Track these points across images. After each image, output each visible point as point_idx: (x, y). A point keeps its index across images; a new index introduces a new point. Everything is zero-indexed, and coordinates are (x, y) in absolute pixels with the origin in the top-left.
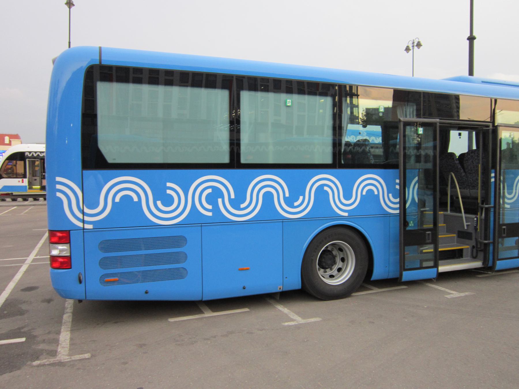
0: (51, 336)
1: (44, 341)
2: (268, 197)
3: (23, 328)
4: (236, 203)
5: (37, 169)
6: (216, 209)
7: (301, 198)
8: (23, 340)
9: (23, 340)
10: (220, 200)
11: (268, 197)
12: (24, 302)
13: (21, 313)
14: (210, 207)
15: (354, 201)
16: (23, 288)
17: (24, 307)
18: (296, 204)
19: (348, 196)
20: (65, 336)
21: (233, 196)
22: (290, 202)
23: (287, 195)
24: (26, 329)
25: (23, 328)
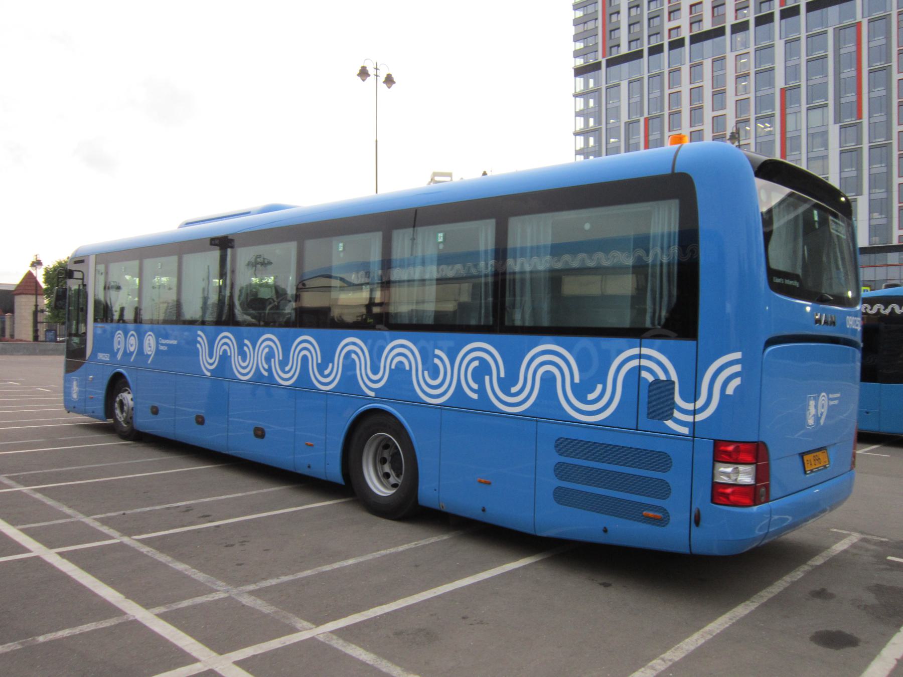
0: (855, 551)
1: (867, 550)
2: (548, 381)
3: (886, 569)
4: (506, 384)
5: (876, 307)
6: (482, 391)
7: (599, 387)
8: (889, 558)
9: (889, 558)
10: (487, 378)
11: (548, 381)
12: (866, 607)
13: (879, 590)
14: (475, 386)
15: (382, 378)
16: (849, 651)
17: (870, 599)
18: (591, 397)
19: (375, 371)
20: (840, 547)
21: (577, 380)
22: (581, 391)
23: (502, 375)
24: (882, 567)
25: (886, 569)
